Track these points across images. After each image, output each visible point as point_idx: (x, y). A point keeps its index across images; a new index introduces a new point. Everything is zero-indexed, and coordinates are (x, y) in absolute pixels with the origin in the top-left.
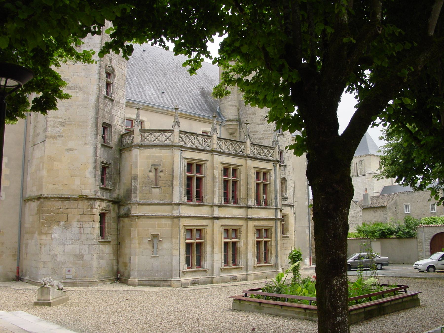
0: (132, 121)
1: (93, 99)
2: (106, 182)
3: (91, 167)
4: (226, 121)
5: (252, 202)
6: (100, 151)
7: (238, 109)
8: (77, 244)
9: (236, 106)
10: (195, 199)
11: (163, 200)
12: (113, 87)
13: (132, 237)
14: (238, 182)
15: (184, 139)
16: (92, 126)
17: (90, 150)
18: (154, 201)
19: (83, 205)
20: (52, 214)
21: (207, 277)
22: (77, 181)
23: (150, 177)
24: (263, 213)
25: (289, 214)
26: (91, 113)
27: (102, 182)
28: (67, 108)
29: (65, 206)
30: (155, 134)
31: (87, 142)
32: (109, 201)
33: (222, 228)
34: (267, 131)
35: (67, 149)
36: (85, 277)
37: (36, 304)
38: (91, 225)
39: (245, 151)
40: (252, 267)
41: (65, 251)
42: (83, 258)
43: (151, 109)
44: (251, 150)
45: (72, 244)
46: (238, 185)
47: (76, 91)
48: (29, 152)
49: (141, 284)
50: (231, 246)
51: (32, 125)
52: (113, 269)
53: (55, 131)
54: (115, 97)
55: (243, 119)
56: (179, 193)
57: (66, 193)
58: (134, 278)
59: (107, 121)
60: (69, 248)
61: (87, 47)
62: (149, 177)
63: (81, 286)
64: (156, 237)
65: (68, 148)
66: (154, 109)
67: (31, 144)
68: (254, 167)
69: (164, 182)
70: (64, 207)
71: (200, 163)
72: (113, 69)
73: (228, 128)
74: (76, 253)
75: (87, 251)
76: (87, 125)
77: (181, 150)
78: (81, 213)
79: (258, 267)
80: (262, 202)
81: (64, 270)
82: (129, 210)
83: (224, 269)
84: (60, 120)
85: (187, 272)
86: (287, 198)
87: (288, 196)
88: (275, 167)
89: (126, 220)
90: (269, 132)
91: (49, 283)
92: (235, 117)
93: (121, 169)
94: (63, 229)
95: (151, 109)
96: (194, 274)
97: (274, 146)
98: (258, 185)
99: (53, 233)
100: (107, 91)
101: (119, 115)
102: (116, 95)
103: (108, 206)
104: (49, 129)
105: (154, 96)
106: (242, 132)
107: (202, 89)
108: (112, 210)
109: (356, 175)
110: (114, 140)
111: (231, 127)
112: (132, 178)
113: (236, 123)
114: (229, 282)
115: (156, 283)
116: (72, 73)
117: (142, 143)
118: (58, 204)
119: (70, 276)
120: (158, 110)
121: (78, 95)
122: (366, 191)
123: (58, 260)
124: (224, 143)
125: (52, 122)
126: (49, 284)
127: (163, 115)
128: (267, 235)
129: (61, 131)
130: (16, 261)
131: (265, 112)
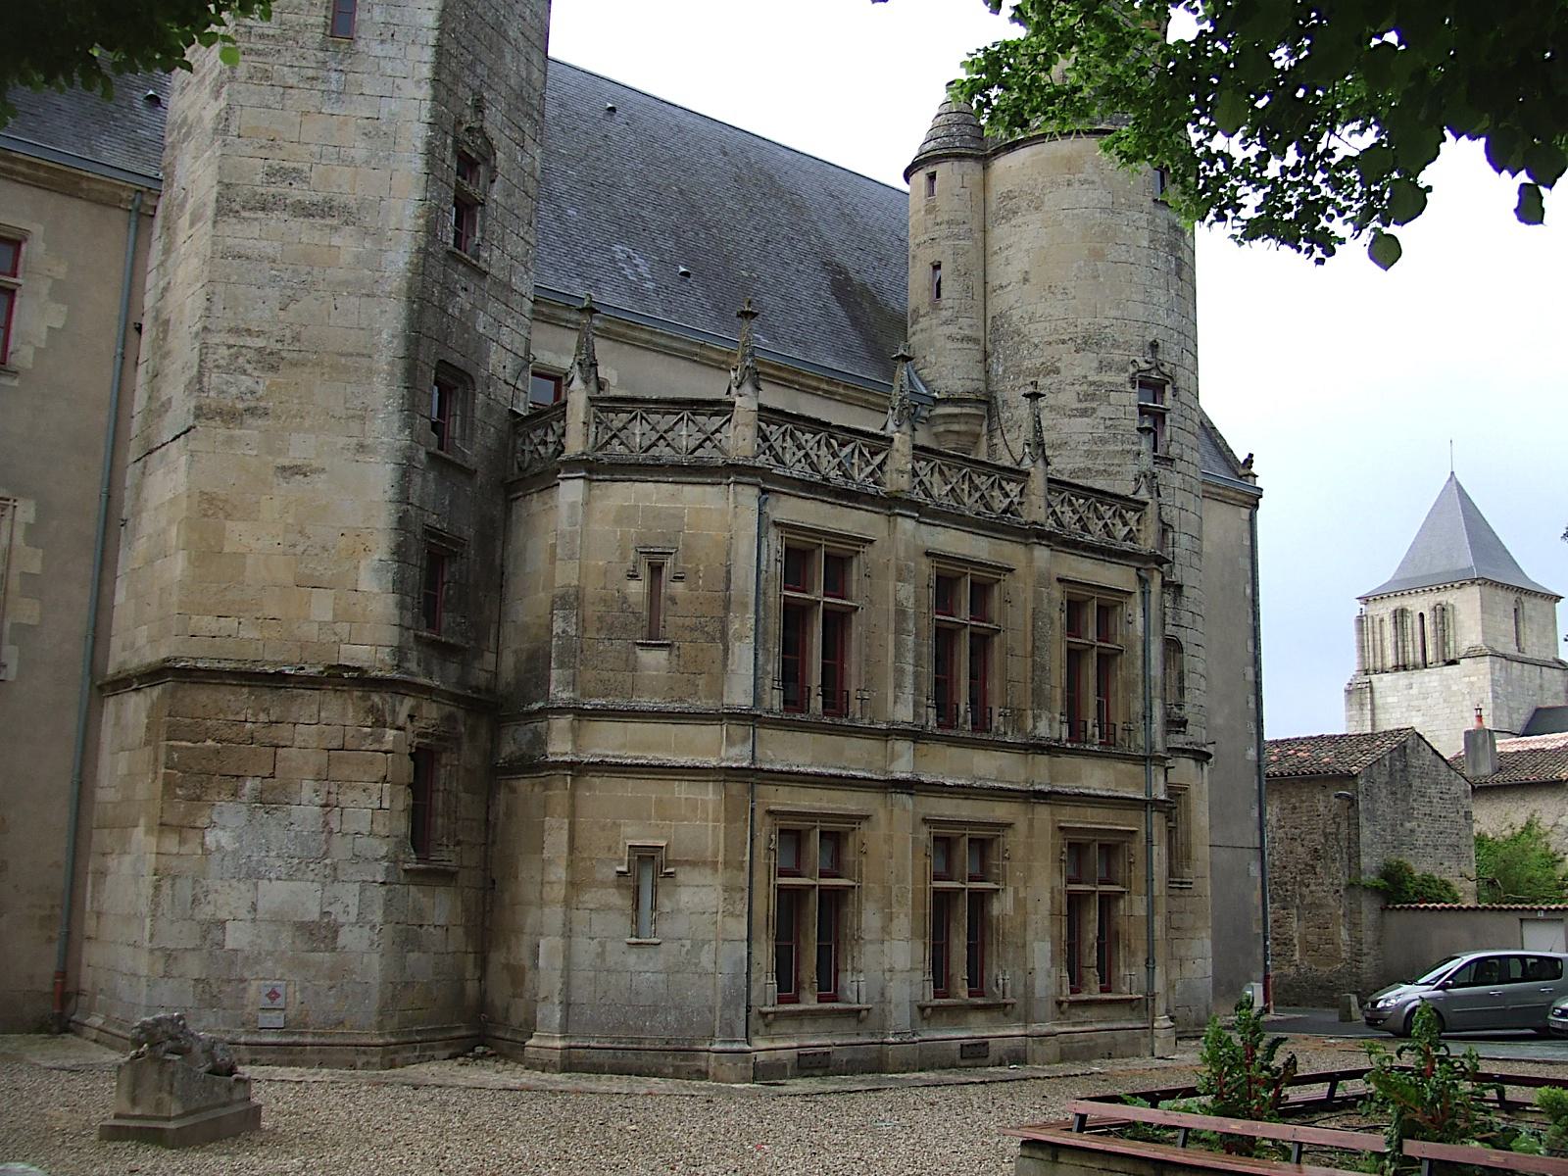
0: (557, 380)
1: (399, 259)
2: (446, 619)
3: (381, 547)
4: (937, 402)
5: (1049, 726)
6: (424, 485)
7: (986, 355)
8: (311, 876)
9: (976, 341)
10: (817, 703)
11: (681, 700)
12: (483, 218)
13: (546, 854)
14: (996, 639)
15: (777, 445)
16: (391, 374)
17: (380, 477)
18: (645, 702)
19: (340, 712)
20: (209, 742)
21: (860, 1040)
22: (322, 606)
23: (631, 600)
24: (1096, 777)
25: (1193, 789)
26: (388, 322)
27: (426, 616)
28: (289, 292)
29: (266, 711)
30: (654, 418)
31: (369, 441)
32: (455, 698)
33: (925, 830)
34: (1103, 441)
35: (284, 469)
36: (341, 1023)
37: (113, 1134)
38: (375, 797)
39: (1024, 510)
40: (1050, 1006)
41: (260, 905)
42: (335, 938)
43: (636, 334)
44: (1050, 505)
45: (290, 877)
46: (996, 656)
47: (329, 221)
48: (128, 483)
49: (568, 1066)
50: (963, 908)
51: (141, 369)
52: (462, 992)
53: (233, 390)
54: (493, 259)
55: (1006, 396)
56: (743, 674)
57: (273, 657)
58: (547, 1041)
59: (455, 359)
60: (275, 893)
61: (383, 42)
62: (625, 600)
63: (321, 1065)
64: (645, 856)
65: (286, 462)
66: (645, 336)
67: (134, 450)
68: (1060, 580)
69: (688, 622)
70: (262, 717)
71: (840, 547)
72: (488, 142)
73: (941, 429)
74: (307, 919)
75: (353, 911)
76: (370, 370)
77: (764, 491)
78: (335, 744)
79: (1072, 1004)
80: (1091, 731)
81: (255, 991)
82: (540, 740)
83: (934, 1008)
84: (260, 343)
85: (779, 1016)
86: (1184, 723)
87: (1188, 712)
88: (1143, 582)
89: (524, 785)
90: (1112, 448)
91: (172, 1038)
92: (970, 385)
93: (510, 568)
94: (252, 812)
95: (636, 334)
96: (808, 1027)
97: (1143, 495)
98: (1074, 656)
99: (213, 825)
100: (458, 237)
101: (506, 339)
102: (497, 252)
103: (450, 718)
104: (214, 379)
105: (650, 285)
106: (1001, 446)
107: (840, 273)
108: (465, 739)
109: (1419, 659)
110: (475, 448)
111: (955, 427)
112: (553, 602)
113: (973, 411)
114: (954, 1066)
115: (647, 1059)
116: (316, 149)
117: (599, 454)
118: (239, 702)
119: (276, 1019)
120: (663, 341)
121: (336, 241)
122: (1480, 717)
123: (230, 944)
124: (941, 472)
125: (224, 351)
126: (169, 1044)
127: (683, 364)
128: (1109, 872)
129: (261, 390)
130: (56, 946)
131: (1095, 364)
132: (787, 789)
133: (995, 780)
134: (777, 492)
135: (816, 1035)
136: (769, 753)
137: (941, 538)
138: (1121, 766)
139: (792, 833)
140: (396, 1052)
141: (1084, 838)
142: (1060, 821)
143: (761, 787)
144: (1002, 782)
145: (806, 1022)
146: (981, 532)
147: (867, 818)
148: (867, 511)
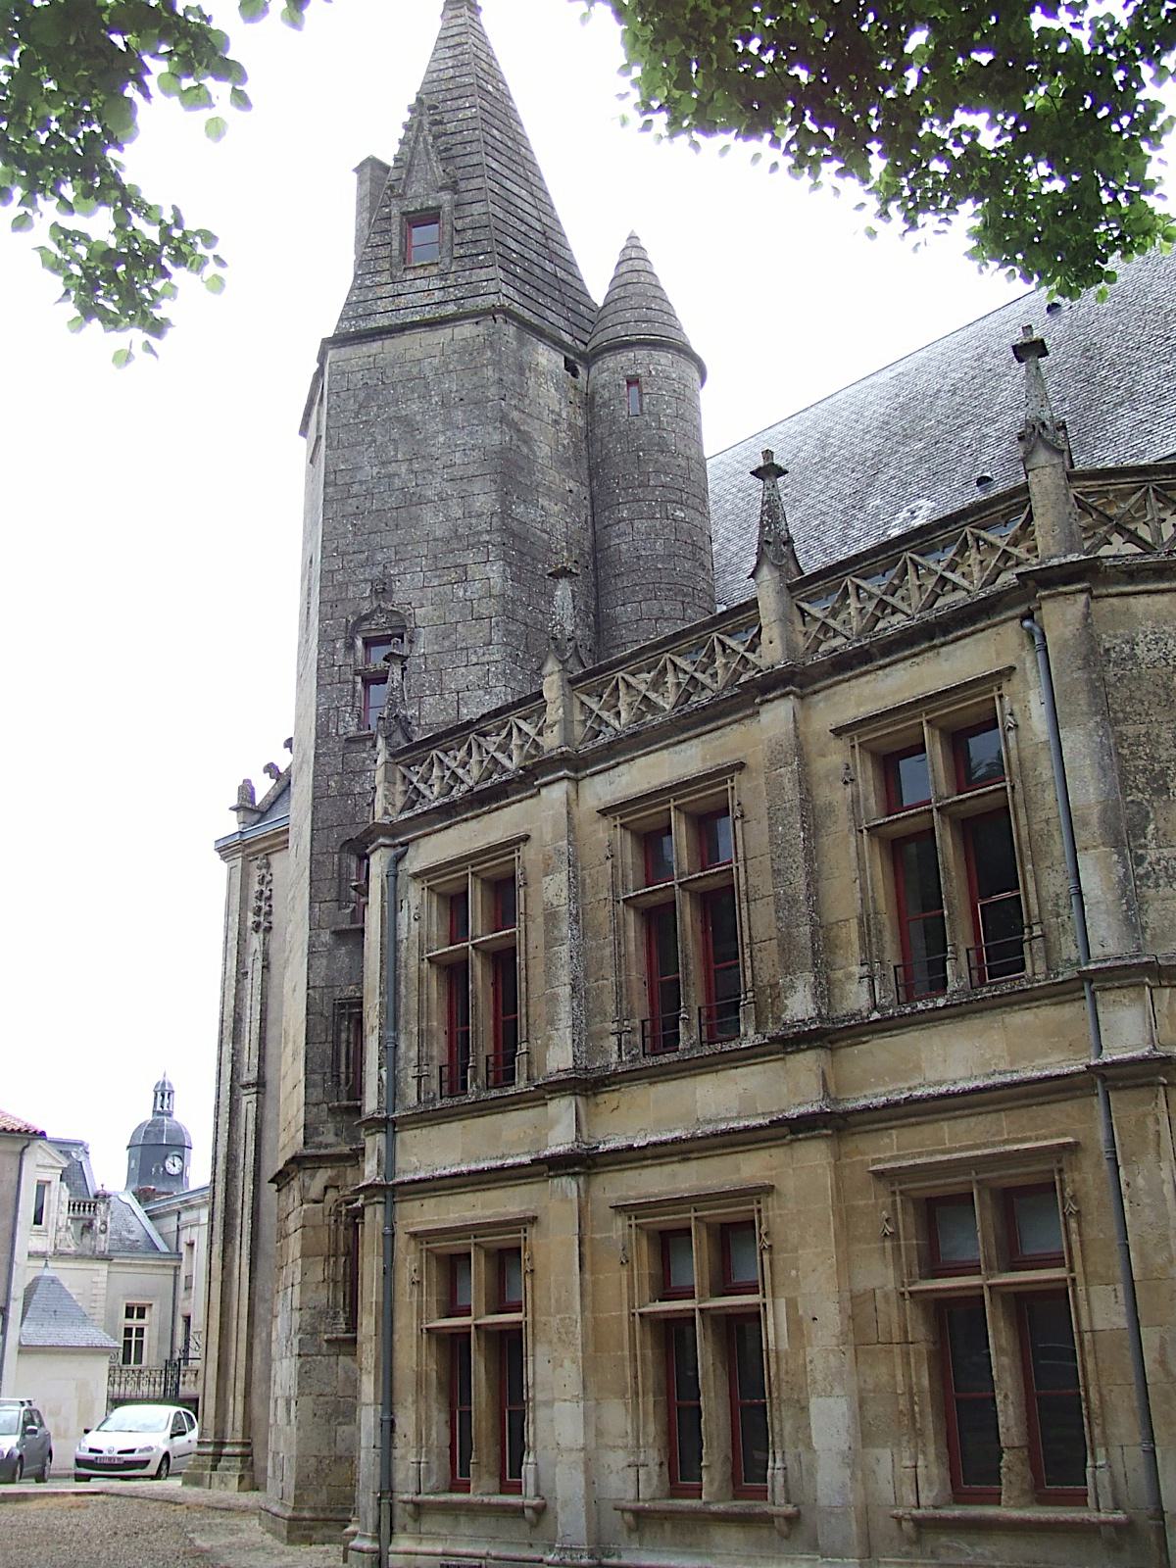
71: (492, 867)
96: (465, 1527)
132: (433, 1201)
133: (739, 1117)
134: (413, 840)
135: (474, 1539)
136: (414, 1159)
137: (625, 779)
138: (1020, 1018)
139: (933, 1208)
140: (311, 1528)
141: (457, 1245)
142: (875, 1161)
143: (405, 1204)
144: (748, 1117)
145: (462, 1519)
146: (685, 736)
147: (533, 1220)
148: (520, 801)
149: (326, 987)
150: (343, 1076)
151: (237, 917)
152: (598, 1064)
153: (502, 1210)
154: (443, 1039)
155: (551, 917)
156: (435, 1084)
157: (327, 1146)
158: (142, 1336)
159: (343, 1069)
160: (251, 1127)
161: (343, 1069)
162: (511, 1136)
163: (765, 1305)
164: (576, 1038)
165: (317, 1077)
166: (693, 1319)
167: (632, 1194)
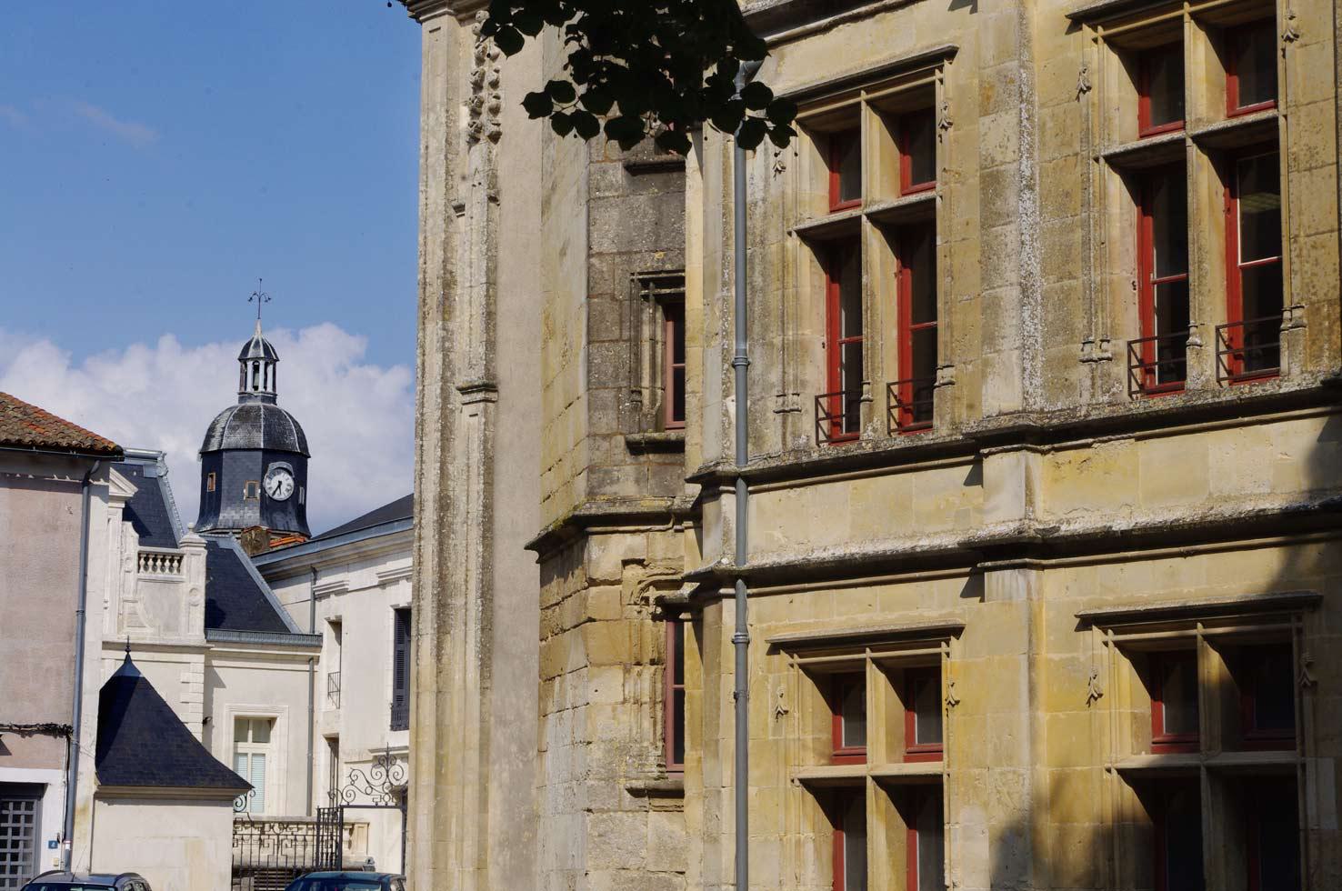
149: (620, 253)
150: (646, 393)
151: (443, 114)
152: (1060, 406)
153: (914, 613)
154: (820, 355)
155: (992, 181)
156: (807, 424)
157: (624, 501)
158: (32, 809)
159: (646, 382)
160: (476, 456)
161: (646, 382)
162: (932, 507)
163: (1304, 766)
164: (1028, 365)
165: (608, 395)
166: (1198, 779)
167: (1110, 598)
